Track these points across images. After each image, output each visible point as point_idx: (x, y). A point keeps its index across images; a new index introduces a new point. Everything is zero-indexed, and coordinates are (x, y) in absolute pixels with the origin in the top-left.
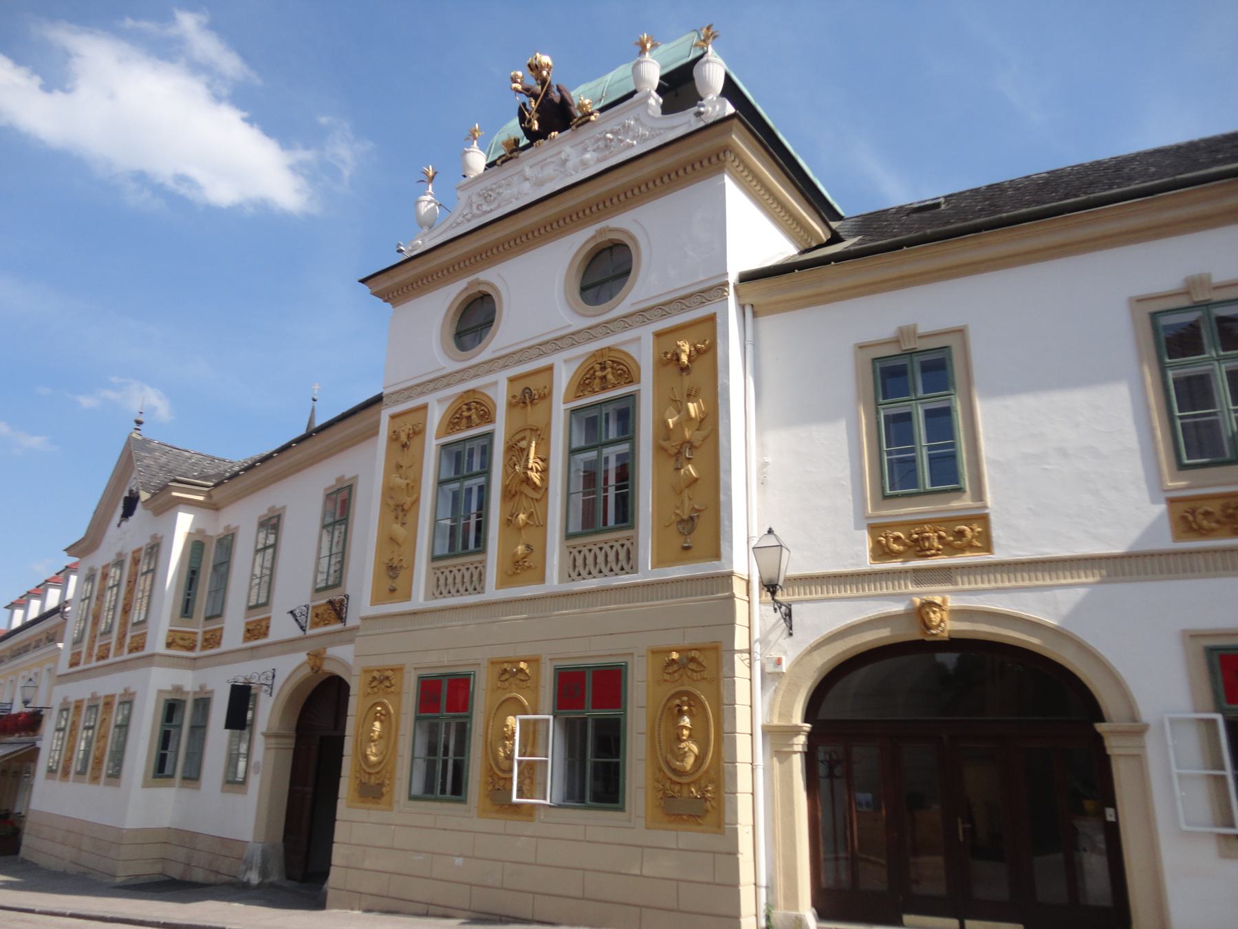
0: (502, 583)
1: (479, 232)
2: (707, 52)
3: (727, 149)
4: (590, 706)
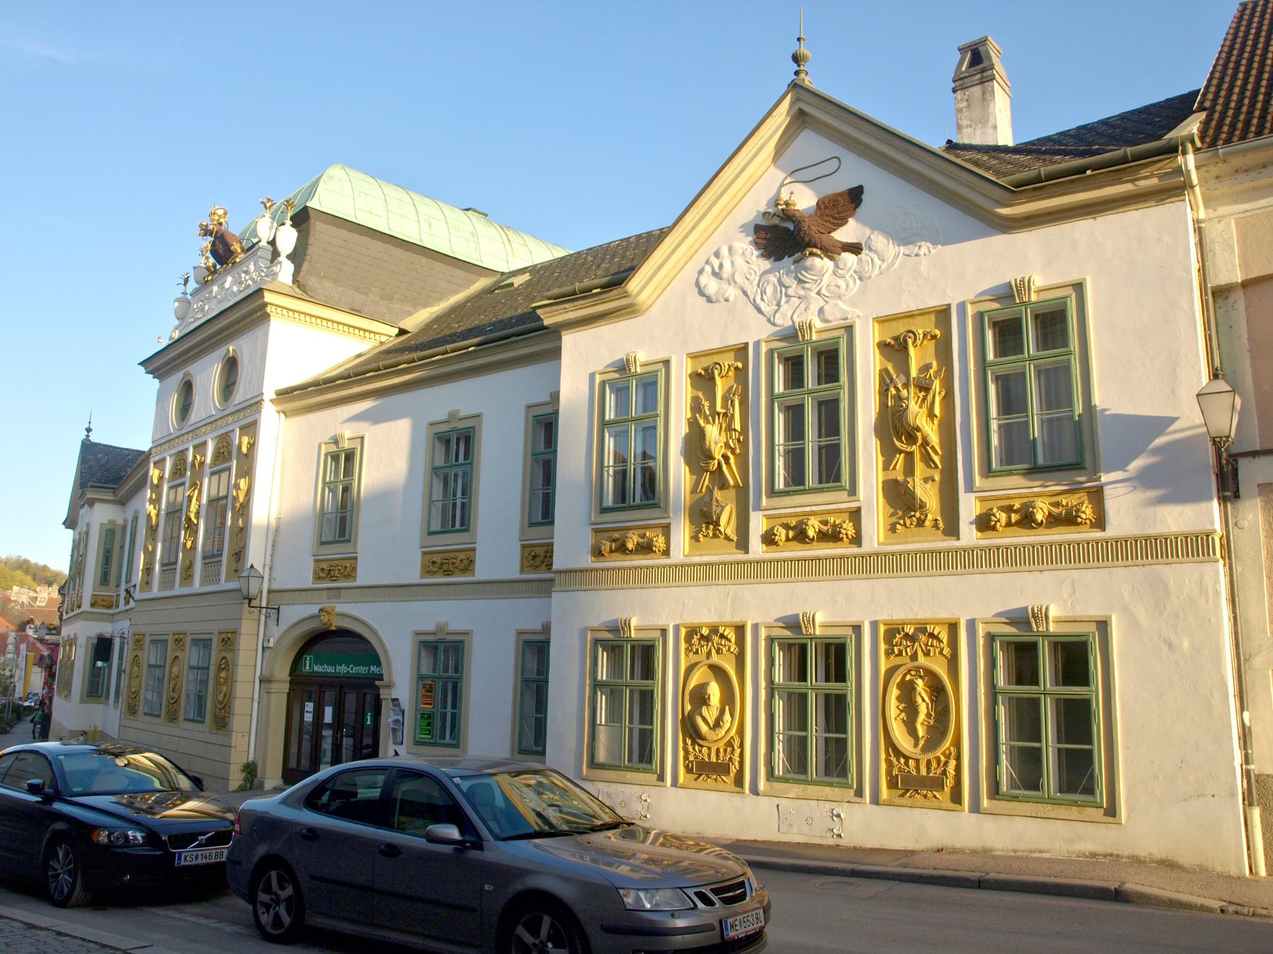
0: (181, 585)
4: (1085, 688)
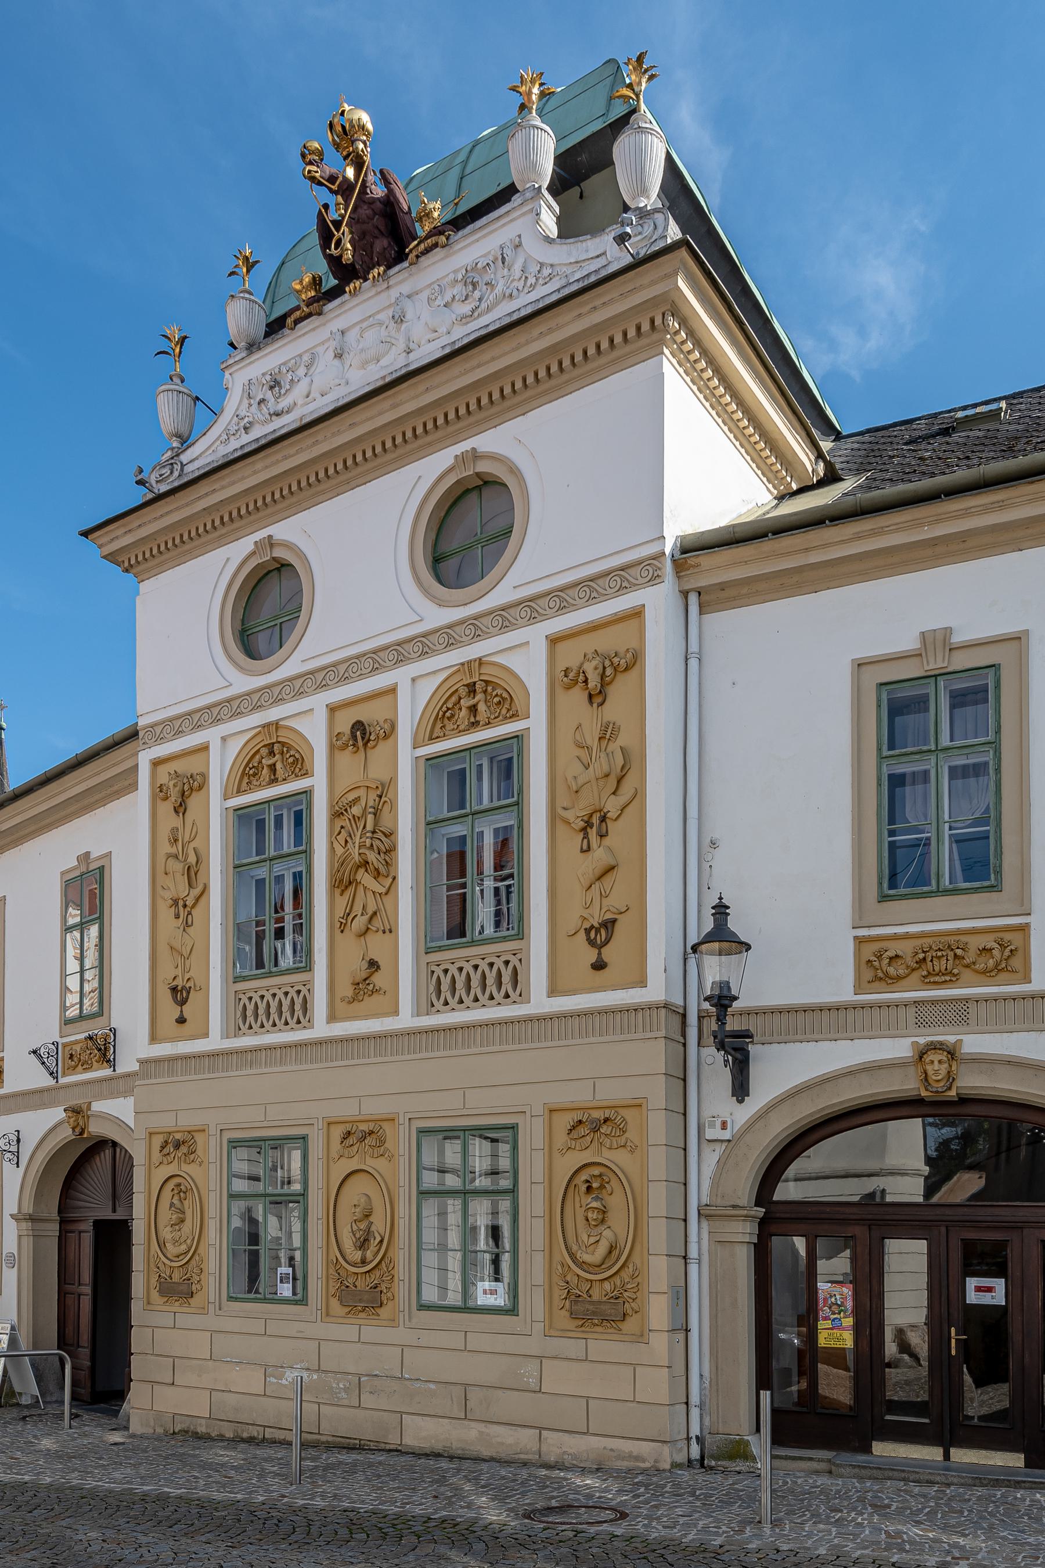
2: (634, 111)
3: (675, 308)
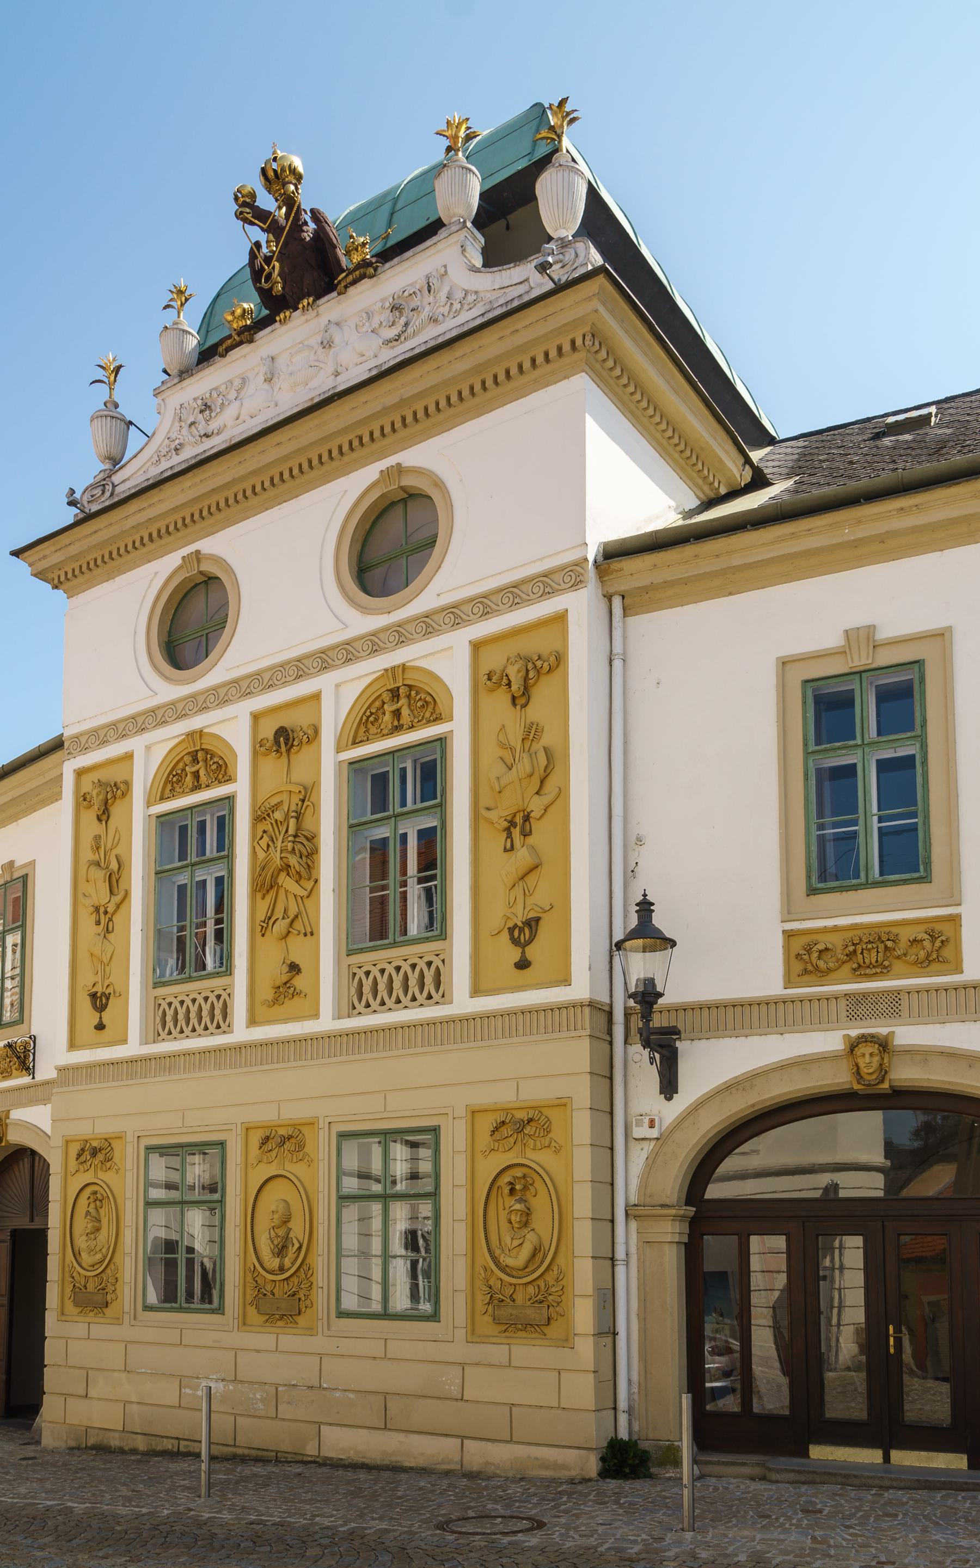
1: (196, 471)
